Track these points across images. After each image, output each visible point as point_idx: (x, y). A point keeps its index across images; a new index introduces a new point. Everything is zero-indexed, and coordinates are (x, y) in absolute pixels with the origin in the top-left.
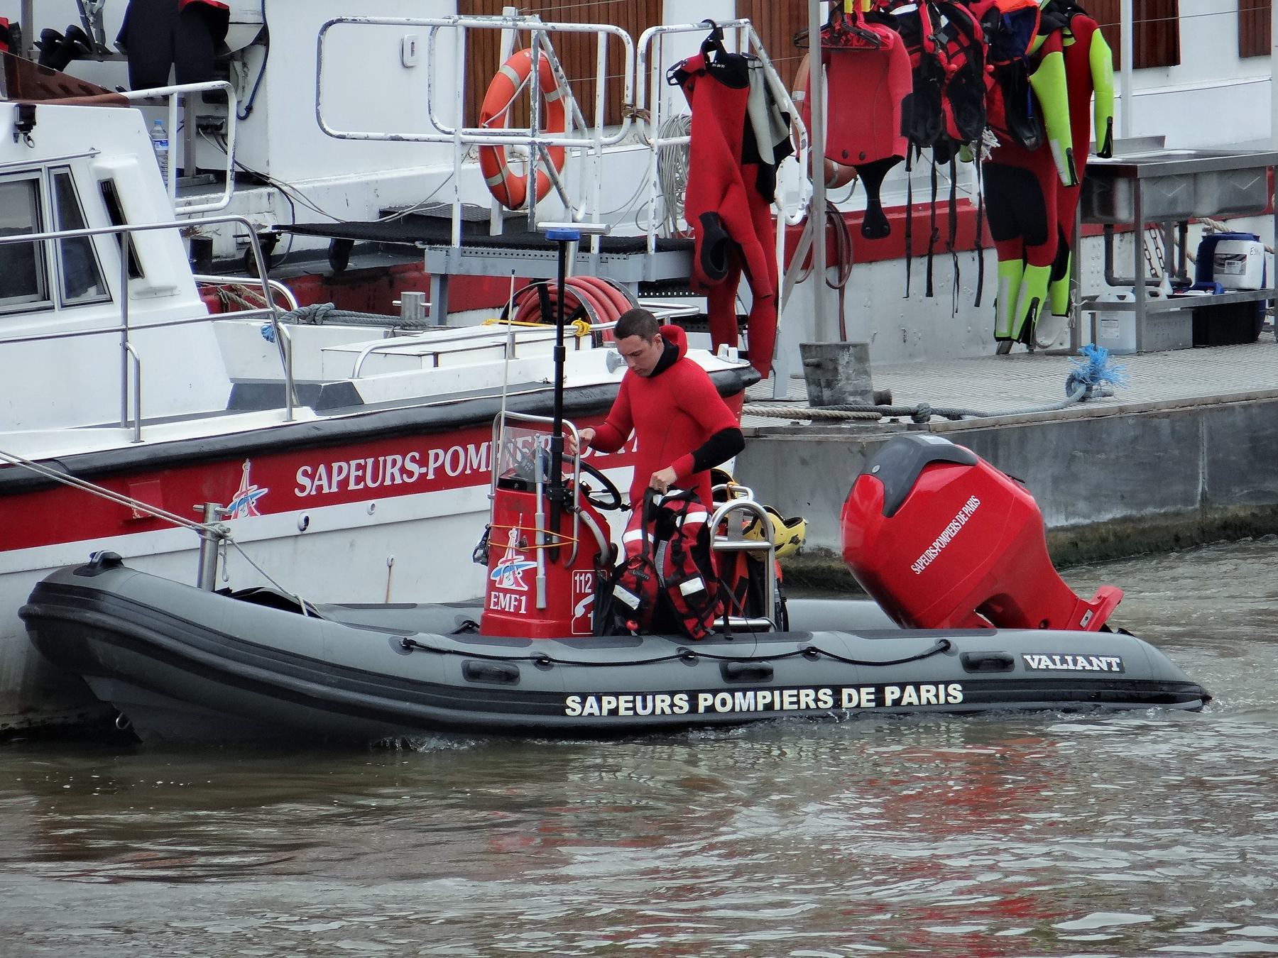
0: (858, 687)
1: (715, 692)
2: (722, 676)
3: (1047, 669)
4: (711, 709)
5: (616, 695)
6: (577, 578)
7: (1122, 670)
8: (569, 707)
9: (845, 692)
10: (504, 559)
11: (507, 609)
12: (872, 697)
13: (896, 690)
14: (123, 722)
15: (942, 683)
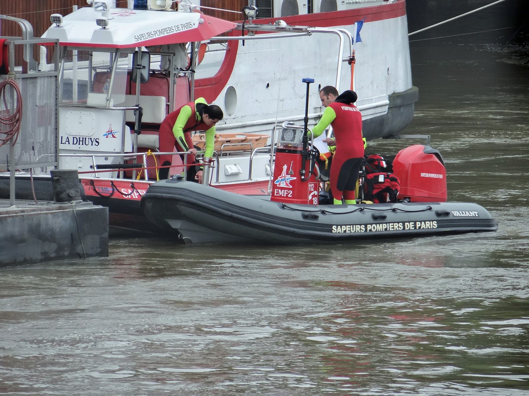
0: (409, 222)
1: (371, 224)
2: (373, 218)
3: (459, 216)
4: (371, 230)
5: (346, 225)
6: (309, 185)
7: (479, 216)
9: (406, 224)
10: (281, 176)
11: (283, 195)
12: (413, 226)
13: (419, 223)
14: (180, 236)
15: (431, 221)
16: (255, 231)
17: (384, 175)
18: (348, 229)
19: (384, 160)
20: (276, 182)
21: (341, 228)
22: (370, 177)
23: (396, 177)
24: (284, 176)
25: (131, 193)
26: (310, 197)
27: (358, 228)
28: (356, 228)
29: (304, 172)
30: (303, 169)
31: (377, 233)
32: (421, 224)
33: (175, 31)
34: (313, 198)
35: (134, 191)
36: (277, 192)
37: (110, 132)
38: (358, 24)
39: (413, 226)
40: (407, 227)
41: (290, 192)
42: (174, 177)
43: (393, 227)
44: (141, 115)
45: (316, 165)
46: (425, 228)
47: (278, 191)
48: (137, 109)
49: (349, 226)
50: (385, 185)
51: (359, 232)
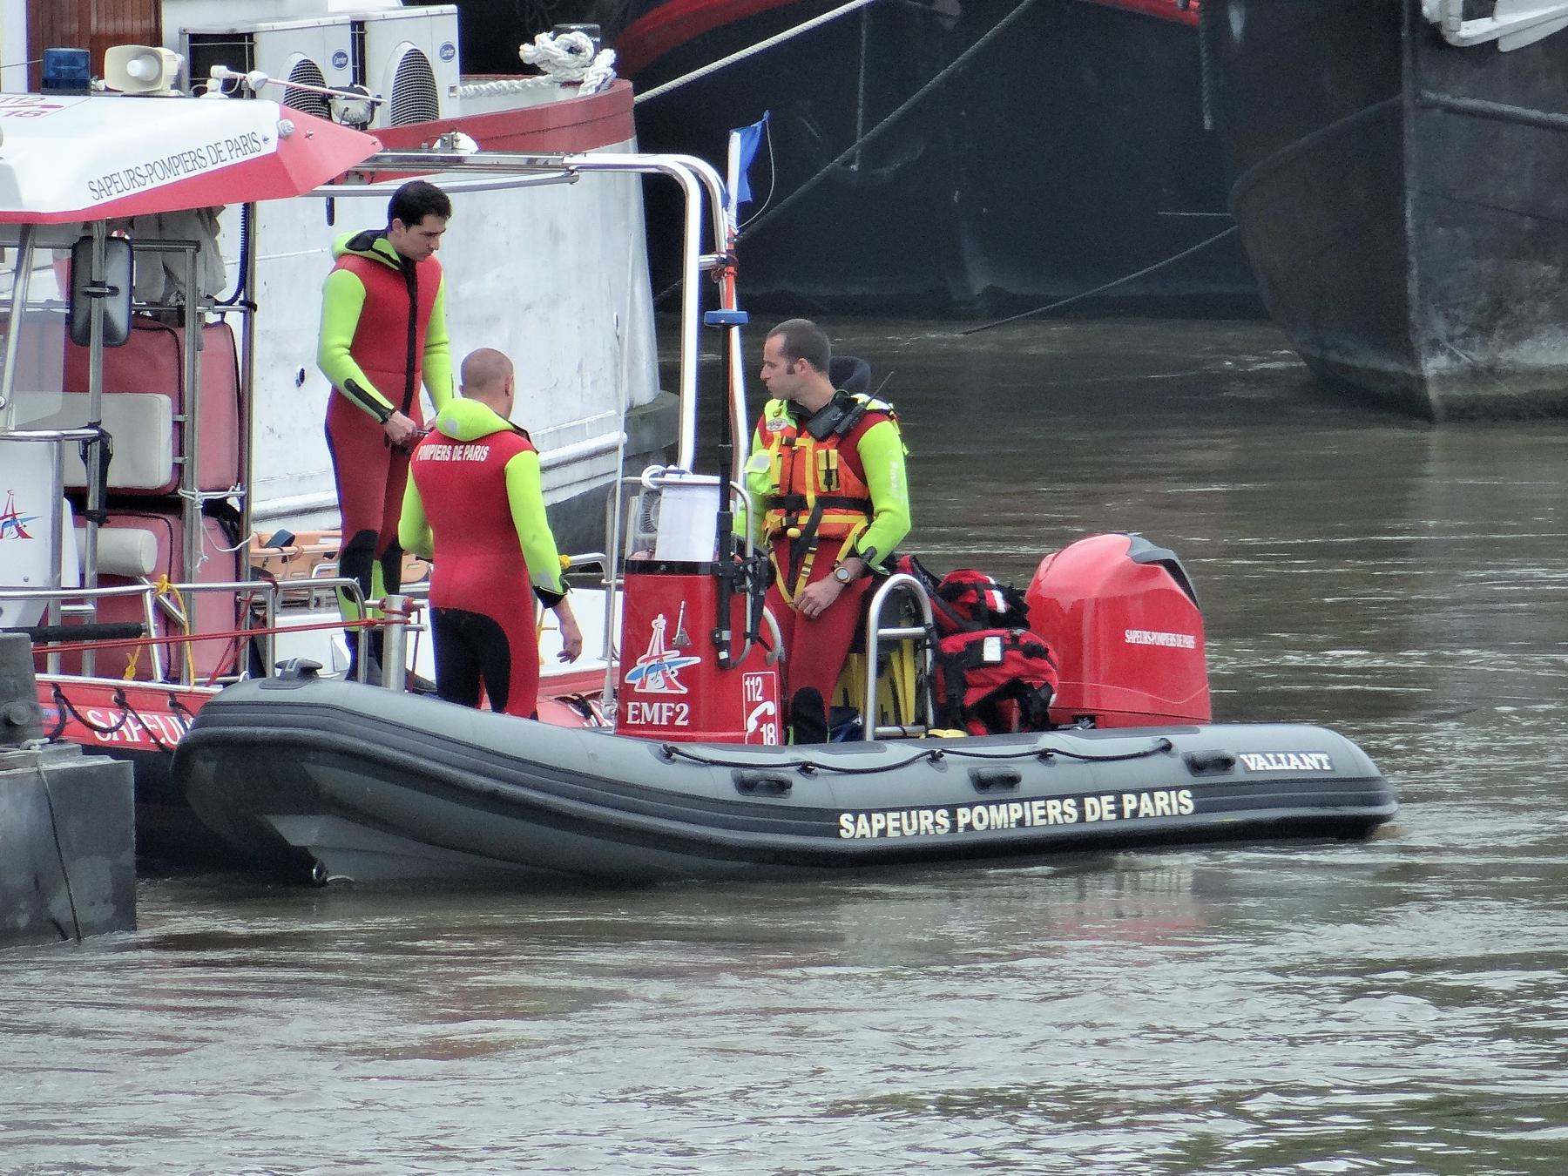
0: (1098, 795)
1: (971, 806)
3: (1298, 771)
4: (969, 827)
5: (884, 811)
6: (747, 683)
7: (1333, 770)
8: (843, 828)
9: (1089, 801)
11: (656, 722)
12: (1112, 807)
13: (1132, 797)
14: (319, 873)
16: (576, 845)
17: (1002, 637)
18: (892, 824)
19: (999, 587)
20: (629, 679)
21: (869, 820)
22: (953, 647)
23: (1043, 643)
24: (656, 653)
25: (119, 725)
26: (751, 724)
27: (925, 820)
28: (918, 819)
29: (726, 635)
30: (722, 623)
31: (990, 836)
32: (1139, 801)
33: (210, 162)
34: (760, 726)
35: (128, 719)
36: (636, 712)
37: (9, 519)
38: (742, 138)
39: (1112, 807)
40: (1093, 813)
41: (682, 707)
42: (287, 669)
43: (1043, 812)
44: (106, 457)
45: (767, 612)
46: (1152, 814)
47: (640, 709)
48: (94, 439)
49: (896, 815)
50: (1007, 672)
51: (932, 832)
